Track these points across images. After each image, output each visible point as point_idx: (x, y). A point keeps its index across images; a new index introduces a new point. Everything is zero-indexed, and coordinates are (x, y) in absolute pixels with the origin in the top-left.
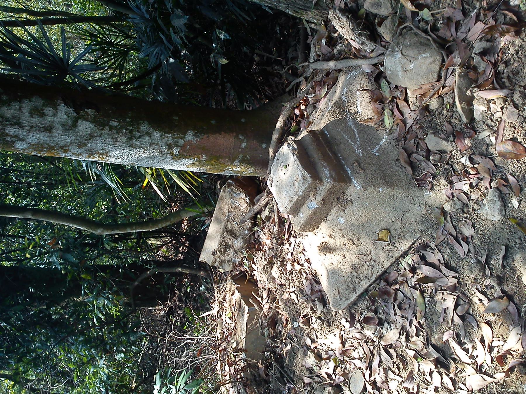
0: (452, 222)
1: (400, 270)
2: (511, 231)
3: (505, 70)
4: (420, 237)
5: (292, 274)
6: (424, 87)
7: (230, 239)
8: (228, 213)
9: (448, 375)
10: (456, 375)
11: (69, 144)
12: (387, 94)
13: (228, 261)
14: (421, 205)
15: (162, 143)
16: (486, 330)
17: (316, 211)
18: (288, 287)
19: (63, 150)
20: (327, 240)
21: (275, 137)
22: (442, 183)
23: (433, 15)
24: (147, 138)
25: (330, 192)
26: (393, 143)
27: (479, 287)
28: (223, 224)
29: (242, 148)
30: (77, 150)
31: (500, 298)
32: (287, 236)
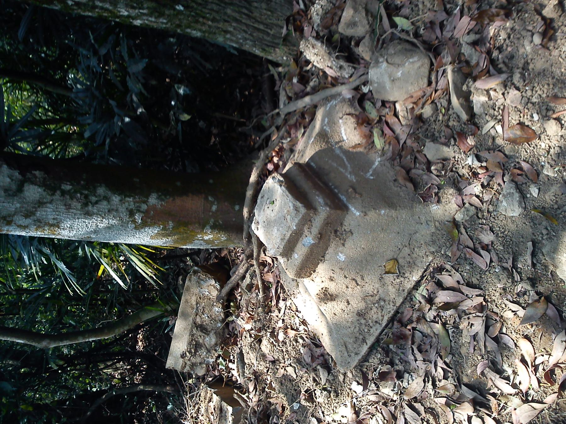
0: (467, 233)
1: (415, 305)
2: (535, 224)
3: (500, 56)
4: (432, 261)
5: (286, 344)
6: (415, 95)
7: (201, 336)
8: (197, 304)
9: (490, 416)
10: (499, 414)
11: (13, 213)
12: (373, 115)
13: (200, 363)
14: (429, 223)
15: (122, 209)
16: (525, 348)
17: (312, 248)
18: (283, 361)
19: (5, 222)
20: (327, 284)
21: (249, 193)
22: (449, 194)
23: (413, 23)
24: (105, 203)
25: (327, 223)
26: (388, 164)
27: (509, 297)
28: (191, 319)
29: (212, 212)
30: (23, 221)
31: (538, 301)
32: (275, 301)
